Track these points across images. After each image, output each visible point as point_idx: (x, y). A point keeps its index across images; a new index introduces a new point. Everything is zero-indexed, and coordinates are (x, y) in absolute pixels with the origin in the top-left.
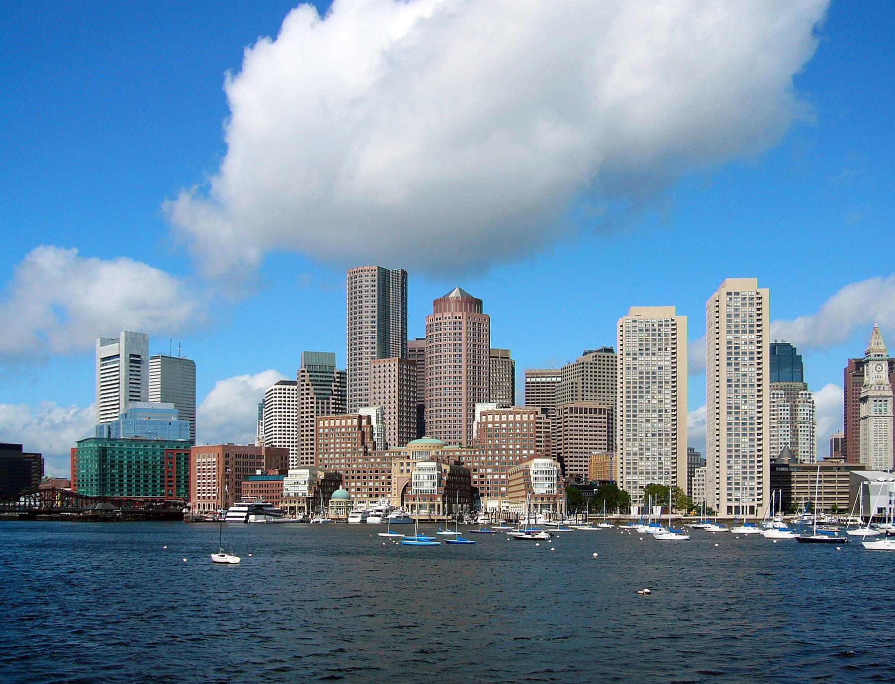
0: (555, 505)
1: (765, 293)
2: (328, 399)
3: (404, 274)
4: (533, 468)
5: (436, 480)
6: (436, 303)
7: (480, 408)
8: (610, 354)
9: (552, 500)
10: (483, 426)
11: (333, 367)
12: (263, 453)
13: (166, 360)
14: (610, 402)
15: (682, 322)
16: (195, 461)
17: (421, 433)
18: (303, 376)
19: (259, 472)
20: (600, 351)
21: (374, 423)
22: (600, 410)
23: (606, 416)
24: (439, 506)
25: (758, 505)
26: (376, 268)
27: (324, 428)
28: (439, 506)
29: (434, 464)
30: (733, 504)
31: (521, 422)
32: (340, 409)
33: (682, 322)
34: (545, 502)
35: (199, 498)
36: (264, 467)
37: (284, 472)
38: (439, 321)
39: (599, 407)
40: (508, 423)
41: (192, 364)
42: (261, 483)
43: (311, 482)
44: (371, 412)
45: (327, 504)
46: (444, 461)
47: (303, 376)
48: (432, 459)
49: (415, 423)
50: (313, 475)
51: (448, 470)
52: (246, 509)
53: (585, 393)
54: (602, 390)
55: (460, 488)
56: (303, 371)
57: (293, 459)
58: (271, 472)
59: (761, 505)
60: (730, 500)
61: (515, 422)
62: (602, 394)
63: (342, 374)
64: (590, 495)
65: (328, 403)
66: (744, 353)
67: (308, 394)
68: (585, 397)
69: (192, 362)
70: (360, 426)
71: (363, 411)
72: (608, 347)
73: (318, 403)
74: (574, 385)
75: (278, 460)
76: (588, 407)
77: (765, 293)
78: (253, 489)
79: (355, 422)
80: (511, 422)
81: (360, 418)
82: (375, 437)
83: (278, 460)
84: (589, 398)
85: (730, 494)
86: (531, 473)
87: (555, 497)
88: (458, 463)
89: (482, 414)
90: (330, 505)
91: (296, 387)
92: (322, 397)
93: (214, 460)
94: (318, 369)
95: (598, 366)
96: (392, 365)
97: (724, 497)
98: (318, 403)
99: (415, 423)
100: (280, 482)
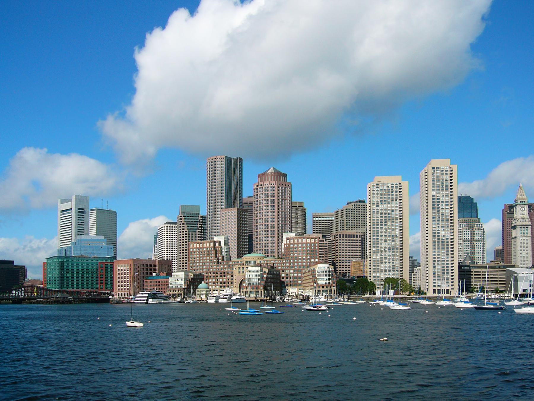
0: (330, 291)
1: (455, 167)
3: (241, 160)
4: (317, 270)
7: (286, 236)
8: (363, 204)
9: (329, 288)
10: (287, 246)
11: (198, 214)
13: (100, 212)
14: (363, 231)
16: (117, 268)
18: (181, 219)
19: (154, 274)
20: (357, 202)
23: (361, 239)
24: (261, 292)
26: (224, 157)
28: (261, 292)
29: (258, 268)
30: (437, 288)
32: (203, 237)
33: (405, 185)
34: (325, 288)
35: (119, 289)
37: (169, 274)
38: (261, 186)
39: (356, 234)
41: (114, 214)
43: (185, 280)
45: (195, 292)
47: (181, 219)
50: (187, 275)
51: (267, 271)
52: (147, 295)
55: (274, 282)
56: (181, 216)
57: (175, 266)
58: (162, 274)
60: (435, 286)
63: (204, 218)
64: (351, 284)
65: (195, 234)
66: (443, 202)
67: (183, 229)
68: (348, 228)
69: (115, 213)
70: (214, 247)
71: (216, 239)
72: (362, 199)
73: (189, 234)
75: (166, 267)
76: (350, 234)
77: (455, 167)
78: (151, 284)
79: (212, 245)
80: (304, 243)
81: (215, 242)
82: (224, 253)
83: (166, 267)
84: (351, 229)
89: (287, 239)
90: (197, 292)
91: (176, 225)
92: (192, 231)
94: (189, 215)
99: (247, 244)
100: (167, 280)
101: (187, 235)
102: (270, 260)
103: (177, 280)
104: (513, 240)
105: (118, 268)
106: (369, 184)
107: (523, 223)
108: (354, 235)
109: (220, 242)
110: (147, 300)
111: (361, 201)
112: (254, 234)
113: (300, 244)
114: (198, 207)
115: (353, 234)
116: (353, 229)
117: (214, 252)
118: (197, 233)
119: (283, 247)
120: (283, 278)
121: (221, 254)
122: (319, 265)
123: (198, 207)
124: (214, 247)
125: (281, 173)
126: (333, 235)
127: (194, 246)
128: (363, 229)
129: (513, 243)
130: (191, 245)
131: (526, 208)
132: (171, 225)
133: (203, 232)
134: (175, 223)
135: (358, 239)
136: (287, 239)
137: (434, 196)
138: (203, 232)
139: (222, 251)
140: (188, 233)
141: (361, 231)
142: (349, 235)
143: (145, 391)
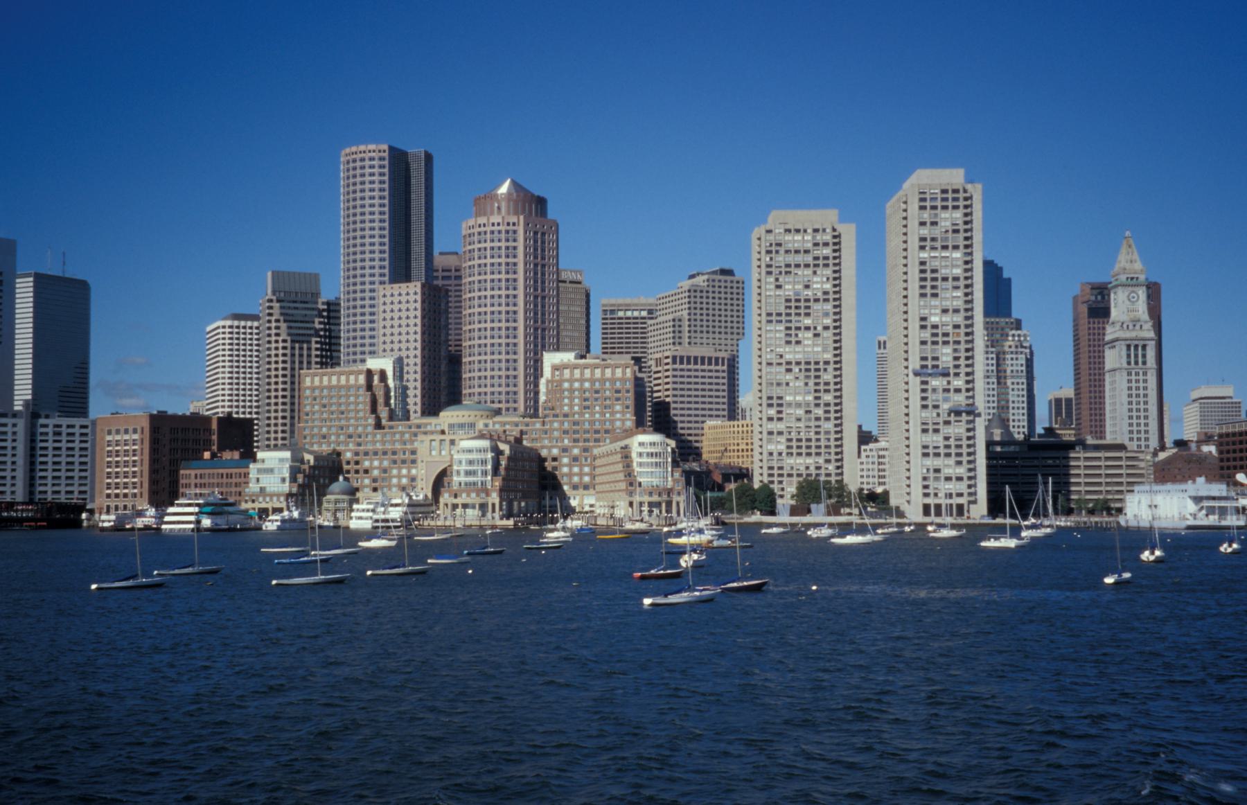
0: (669, 504)
1: (976, 191)
2: (309, 342)
3: (429, 158)
4: (635, 450)
5: (489, 467)
6: (1156, 284)
7: (550, 359)
8: (729, 278)
9: (665, 497)
10: (556, 387)
11: (316, 295)
12: (214, 426)
13: (43, 284)
14: (729, 348)
15: (849, 234)
16: (103, 439)
17: (454, 398)
18: (271, 308)
19: (207, 455)
20: (714, 273)
21: (391, 383)
22: (717, 359)
23: (725, 368)
24: (493, 505)
25: (970, 502)
26: (385, 147)
27: (313, 389)
28: (493, 505)
29: (485, 443)
30: (931, 501)
31: (613, 381)
32: (329, 357)
33: (849, 234)
34: (655, 498)
35: (108, 496)
36: (215, 448)
37: (249, 456)
38: (482, 229)
39: (714, 355)
40: (592, 381)
41: (83, 286)
42: (229, 471)
43: (294, 472)
44: (384, 364)
45: (320, 504)
46: (499, 439)
47: (271, 308)
48: (481, 436)
49: (443, 383)
50: (297, 459)
51: (507, 452)
52: (196, 509)
53: (693, 334)
54: (717, 330)
55: (532, 483)
56: (271, 301)
57: (259, 433)
58: (227, 455)
59: (975, 502)
60: (926, 495)
61: (603, 381)
62: (717, 336)
63: (333, 309)
64: (712, 485)
65: (309, 349)
66: (945, 279)
67: (277, 335)
68: (693, 341)
69: (83, 286)
70: (369, 387)
71: (373, 364)
72: (727, 267)
73: (293, 348)
74: (677, 323)
75: (238, 436)
76: (699, 355)
77: (976, 191)
78: (198, 481)
79: (362, 379)
80: (598, 380)
81: (369, 373)
82: (392, 401)
83: (238, 436)
84: (698, 341)
85: (926, 487)
86: (634, 455)
87: (669, 492)
88: (518, 441)
89: (555, 368)
90: (325, 505)
91: (256, 324)
92: (298, 339)
93: (136, 437)
94: (299, 298)
95: (711, 295)
96: (410, 294)
97: (917, 491)
98: (293, 348)
99: (443, 383)
100: (243, 471)
101: (288, 352)
102: (509, 423)
103: (271, 471)
104: (1108, 377)
105: (109, 438)
106: (756, 229)
107: (1133, 334)
108: (710, 359)
109: (383, 374)
110: (198, 522)
111: (724, 272)
112: (466, 352)
113: (577, 380)
114: (315, 278)
115: (707, 354)
116: (704, 341)
117: (368, 399)
118: (314, 346)
119: (543, 388)
120: (348, 463)
121: (387, 403)
122: (710, 423)
123: (315, 278)
124: (369, 387)
125: (533, 195)
126: (658, 356)
127: (314, 380)
128: (729, 342)
129: (1107, 383)
130: (308, 380)
131: (1142, 293)
132: (243, 323)
133: (330, 344)
134: (255, 318)
135: (719, 368)
136: (555, 368)
137: (923, 263)
138: (330, 344)
139: (387, 397)
140: (288, 345)
141: (723, 347)
142: (696, 358)
143: (930, 767)
